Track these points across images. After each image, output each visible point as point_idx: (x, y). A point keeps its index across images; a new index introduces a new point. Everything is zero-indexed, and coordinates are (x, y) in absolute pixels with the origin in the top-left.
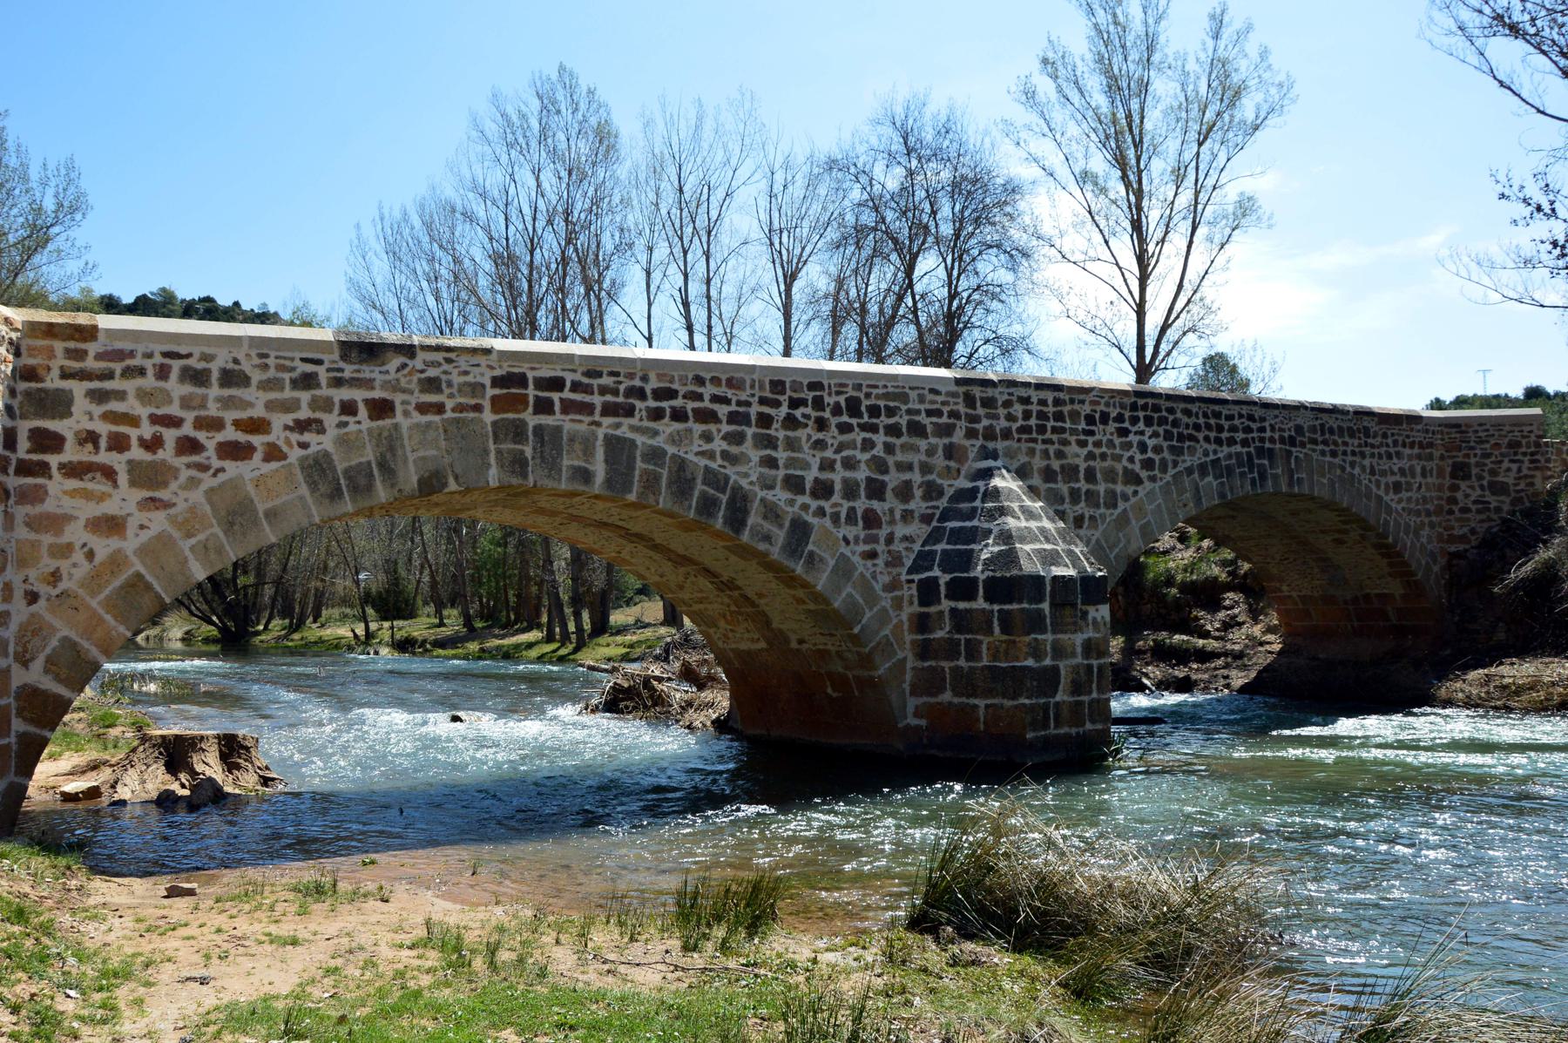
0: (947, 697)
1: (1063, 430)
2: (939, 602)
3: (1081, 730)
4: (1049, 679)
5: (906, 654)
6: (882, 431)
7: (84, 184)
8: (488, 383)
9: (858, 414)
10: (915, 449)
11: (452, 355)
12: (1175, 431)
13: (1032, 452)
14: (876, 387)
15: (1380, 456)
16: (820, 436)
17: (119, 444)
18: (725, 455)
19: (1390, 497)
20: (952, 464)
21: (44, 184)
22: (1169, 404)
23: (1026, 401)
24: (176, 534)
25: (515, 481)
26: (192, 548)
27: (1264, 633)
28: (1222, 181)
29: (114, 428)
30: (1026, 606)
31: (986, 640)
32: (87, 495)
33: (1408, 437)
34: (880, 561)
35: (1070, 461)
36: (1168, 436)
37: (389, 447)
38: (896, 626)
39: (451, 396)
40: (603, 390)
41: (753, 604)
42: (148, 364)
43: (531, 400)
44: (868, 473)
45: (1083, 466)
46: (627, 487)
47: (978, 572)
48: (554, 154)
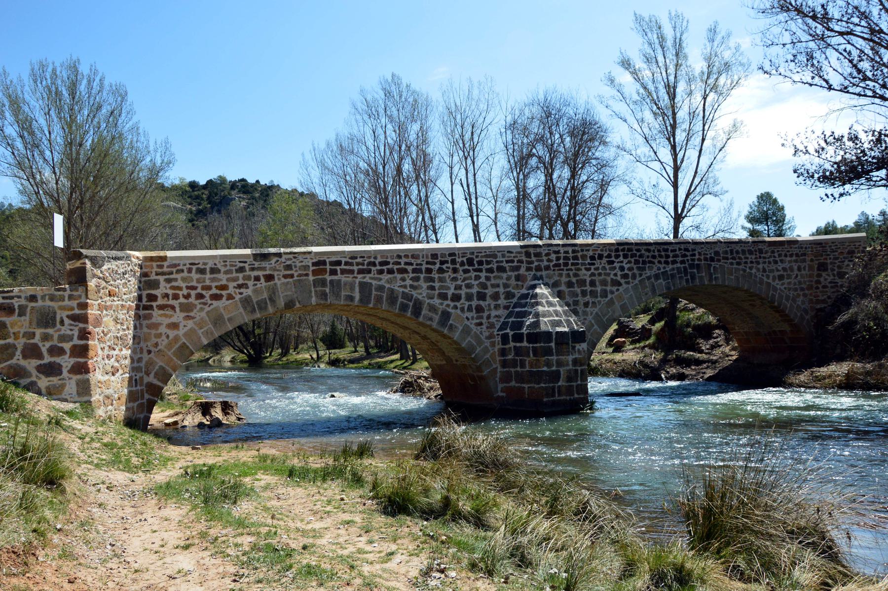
0: (513, 383)
1: (578, 264)
2: (509, 343)
3: (572, 398)
4: (555, 376)
5: (497, 365)
6: (484, 271)
7: (173, 149)
8: (311, 265)
9: (473, 265)
10: (501, 278)
11: (296, 255)
12: (641, 260)
13: (561, 275)
14: (481, 253)
15: (770, 263)
16: (455, 275)
17: (176, 297)
18: (411, 286)
19: (777, 284)
20: (520, 283)
21: (156, 151)
22: (637, 247)
23: (558, 252)
24: (197, 328)
25: (322, 302)
26: (202, 333)
27: (730, 350)
28: (716, 117)
29: (174, 292)
30: (542, 344)
31: (528, 359)
32: (166, 316)
33: (788, 251)
34: (484, 327)
35: (581, 278)
36: (637, 262)
37: (273, 292)
38: (492, 354)
39: (296, 271)
40: (358, 264)
41: (436, 345)
42: (185, 268)
43: (328, 270)
44: (478, 290)
45: (588, 280)
46: (369, 302)
47: (524, 330)
48: (391, 118)
